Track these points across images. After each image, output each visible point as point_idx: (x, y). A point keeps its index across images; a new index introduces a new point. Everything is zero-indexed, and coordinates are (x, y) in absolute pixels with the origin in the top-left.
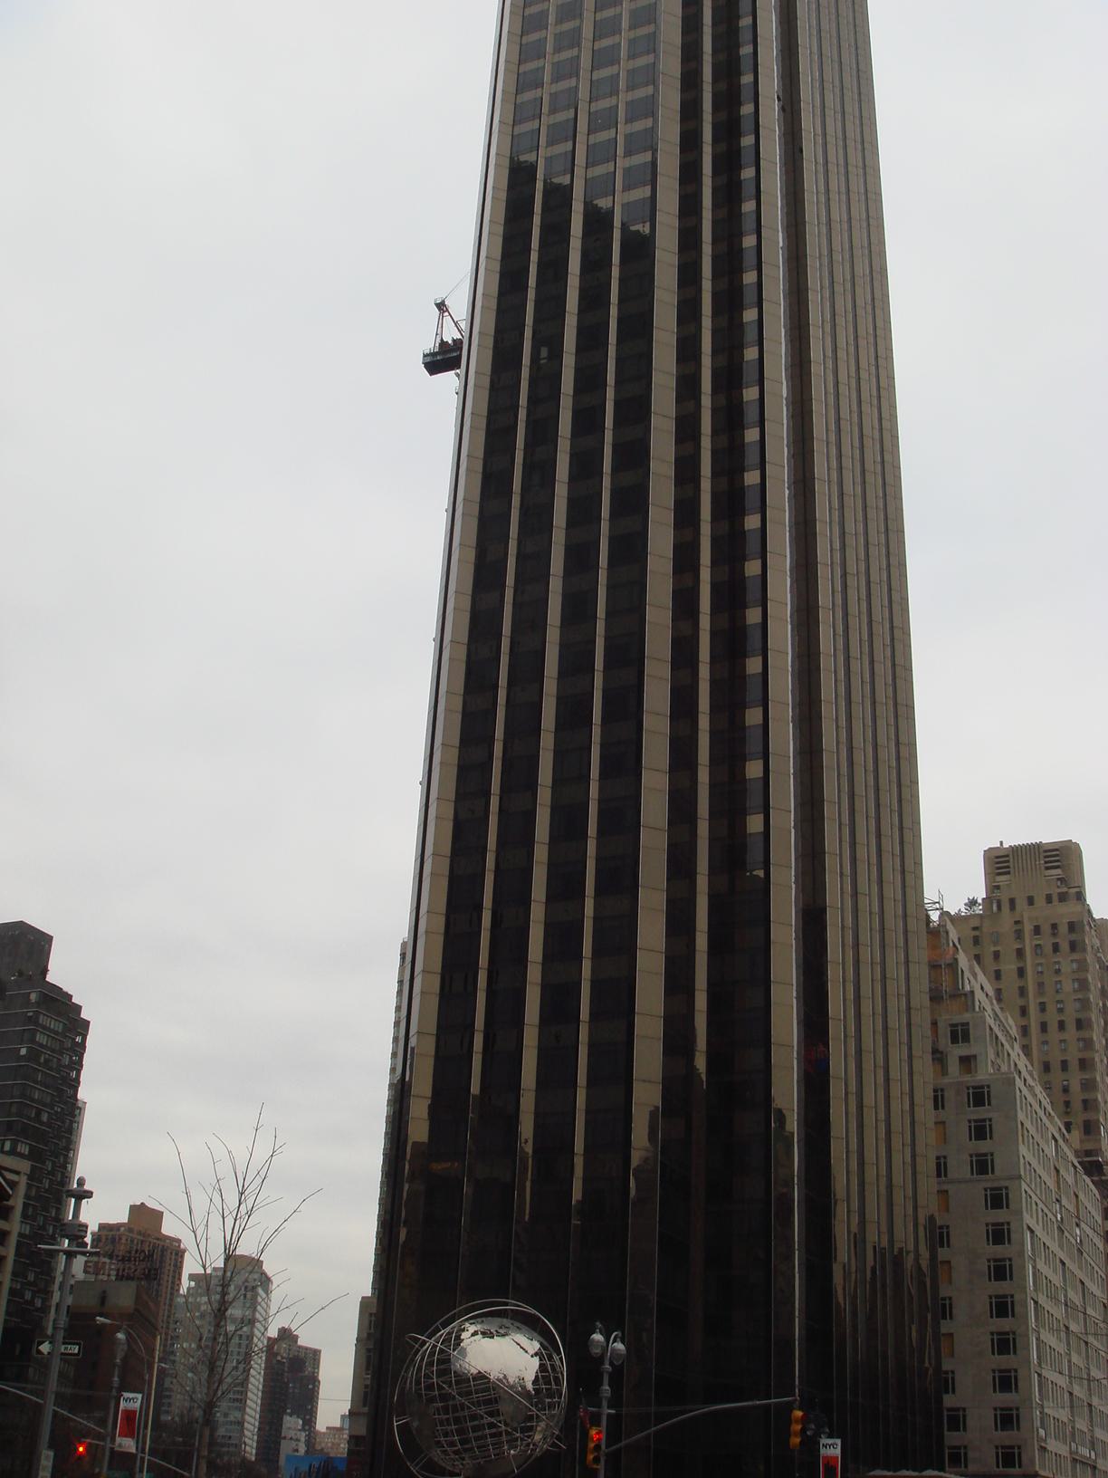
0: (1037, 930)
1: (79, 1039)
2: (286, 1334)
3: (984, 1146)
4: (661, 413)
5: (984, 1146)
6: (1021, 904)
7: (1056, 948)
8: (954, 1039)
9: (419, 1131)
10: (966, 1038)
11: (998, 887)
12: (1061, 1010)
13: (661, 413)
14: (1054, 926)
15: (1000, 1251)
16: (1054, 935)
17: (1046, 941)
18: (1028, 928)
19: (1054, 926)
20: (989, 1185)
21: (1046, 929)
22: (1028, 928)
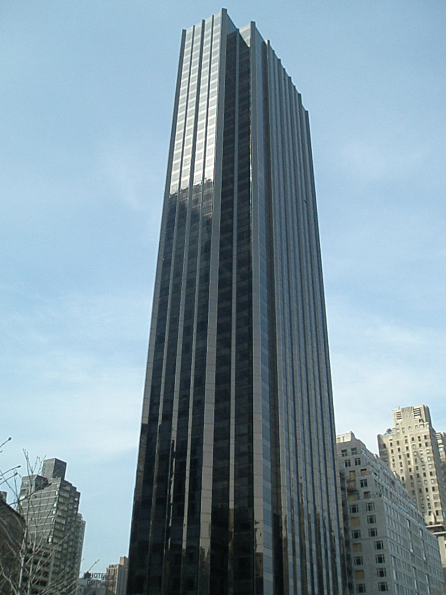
0: (413, 439)
1: (76, 499)
2: (87, 575)
3: (373, 526)
4: (235, 284)
5: (373, 526)
6: (406, 430)
7: (420, 445)
8: (362, 486)
9: (251, 352)
10: (366, 485)
11: (397, 424)
12: (424, 469)
13: (235, 284)
14: (419, 437)
15: (380, 565)
16: (420, 440)
17: (417, 443)
18: (409, 439)
19: (419, 437)
20: (376, 540)
21: (416, 439)
22: (409, 439)
